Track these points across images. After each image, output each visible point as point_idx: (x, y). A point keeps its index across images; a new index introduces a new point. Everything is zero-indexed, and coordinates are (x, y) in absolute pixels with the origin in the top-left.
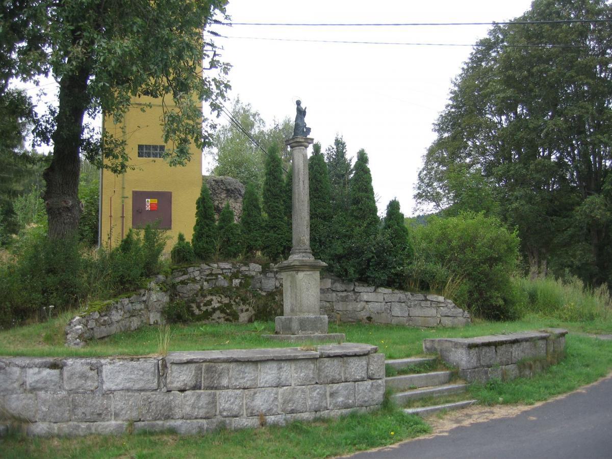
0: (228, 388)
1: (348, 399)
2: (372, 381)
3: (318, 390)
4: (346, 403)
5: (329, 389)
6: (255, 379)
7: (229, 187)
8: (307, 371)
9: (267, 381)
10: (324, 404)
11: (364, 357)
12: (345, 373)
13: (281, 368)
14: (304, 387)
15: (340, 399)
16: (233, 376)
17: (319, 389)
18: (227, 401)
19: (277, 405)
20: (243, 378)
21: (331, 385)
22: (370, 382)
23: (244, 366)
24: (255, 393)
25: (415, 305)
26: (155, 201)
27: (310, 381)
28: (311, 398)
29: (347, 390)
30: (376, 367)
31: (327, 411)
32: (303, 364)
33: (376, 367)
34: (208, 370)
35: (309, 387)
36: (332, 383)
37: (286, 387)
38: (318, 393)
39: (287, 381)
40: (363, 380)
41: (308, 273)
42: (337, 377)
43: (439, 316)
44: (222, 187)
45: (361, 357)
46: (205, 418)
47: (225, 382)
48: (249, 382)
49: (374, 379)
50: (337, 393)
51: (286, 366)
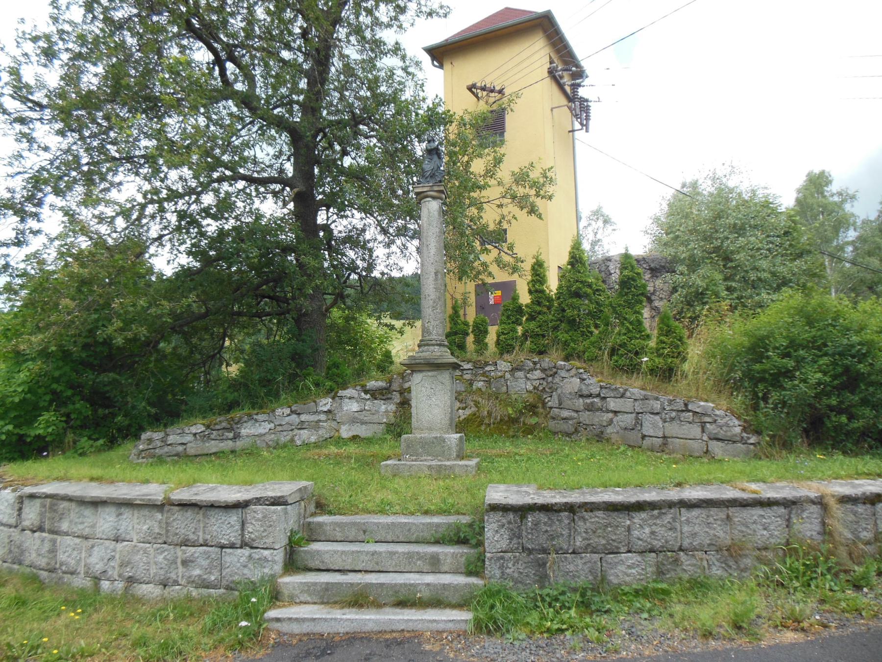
0: (67, 534)
1: (210, 573)
2: (252, 551)
3: (166, 553)
4: (205, 579)
5: (181, 553)
6: (93, 526)
7: (652, 265)
8: (151, 523)
9: (103, 531)
10: (173, 576)
11: (234, 511)
12: (205, 533)
13: (121, 514)
14: (148, 545)
15: (197, 572)
16: (74, 520)
17: (170, 552)
18: (68, 552)
19: (114, 568)
20: (82, 523)
21: (183, 548)
22: (246, 551)
23: (83, 508)
24: (93, 547)
25: (672, 419)
26: (499, 293)
27: (155, 538)
28: (156, 563)
29: (207, 558)
30: (258, 527)
31: (177, 587)
32: (146, 512)
33: (258, 527)
34: (52, 506)
35: (155, 546)
36: (186, 545)
37: (126, 543)
38: (165, 558)
39: (129, 534)
40: (232, 546)
41: (430, 374)
42: (192, 537)
43: (705, 438)
44: (645, 266)
45: (186, 508)
46: (46, 570)
47: (64, 526)
48: (87, 529)
49: (257, 548)
50: (193, 562)
51: (127, 513)
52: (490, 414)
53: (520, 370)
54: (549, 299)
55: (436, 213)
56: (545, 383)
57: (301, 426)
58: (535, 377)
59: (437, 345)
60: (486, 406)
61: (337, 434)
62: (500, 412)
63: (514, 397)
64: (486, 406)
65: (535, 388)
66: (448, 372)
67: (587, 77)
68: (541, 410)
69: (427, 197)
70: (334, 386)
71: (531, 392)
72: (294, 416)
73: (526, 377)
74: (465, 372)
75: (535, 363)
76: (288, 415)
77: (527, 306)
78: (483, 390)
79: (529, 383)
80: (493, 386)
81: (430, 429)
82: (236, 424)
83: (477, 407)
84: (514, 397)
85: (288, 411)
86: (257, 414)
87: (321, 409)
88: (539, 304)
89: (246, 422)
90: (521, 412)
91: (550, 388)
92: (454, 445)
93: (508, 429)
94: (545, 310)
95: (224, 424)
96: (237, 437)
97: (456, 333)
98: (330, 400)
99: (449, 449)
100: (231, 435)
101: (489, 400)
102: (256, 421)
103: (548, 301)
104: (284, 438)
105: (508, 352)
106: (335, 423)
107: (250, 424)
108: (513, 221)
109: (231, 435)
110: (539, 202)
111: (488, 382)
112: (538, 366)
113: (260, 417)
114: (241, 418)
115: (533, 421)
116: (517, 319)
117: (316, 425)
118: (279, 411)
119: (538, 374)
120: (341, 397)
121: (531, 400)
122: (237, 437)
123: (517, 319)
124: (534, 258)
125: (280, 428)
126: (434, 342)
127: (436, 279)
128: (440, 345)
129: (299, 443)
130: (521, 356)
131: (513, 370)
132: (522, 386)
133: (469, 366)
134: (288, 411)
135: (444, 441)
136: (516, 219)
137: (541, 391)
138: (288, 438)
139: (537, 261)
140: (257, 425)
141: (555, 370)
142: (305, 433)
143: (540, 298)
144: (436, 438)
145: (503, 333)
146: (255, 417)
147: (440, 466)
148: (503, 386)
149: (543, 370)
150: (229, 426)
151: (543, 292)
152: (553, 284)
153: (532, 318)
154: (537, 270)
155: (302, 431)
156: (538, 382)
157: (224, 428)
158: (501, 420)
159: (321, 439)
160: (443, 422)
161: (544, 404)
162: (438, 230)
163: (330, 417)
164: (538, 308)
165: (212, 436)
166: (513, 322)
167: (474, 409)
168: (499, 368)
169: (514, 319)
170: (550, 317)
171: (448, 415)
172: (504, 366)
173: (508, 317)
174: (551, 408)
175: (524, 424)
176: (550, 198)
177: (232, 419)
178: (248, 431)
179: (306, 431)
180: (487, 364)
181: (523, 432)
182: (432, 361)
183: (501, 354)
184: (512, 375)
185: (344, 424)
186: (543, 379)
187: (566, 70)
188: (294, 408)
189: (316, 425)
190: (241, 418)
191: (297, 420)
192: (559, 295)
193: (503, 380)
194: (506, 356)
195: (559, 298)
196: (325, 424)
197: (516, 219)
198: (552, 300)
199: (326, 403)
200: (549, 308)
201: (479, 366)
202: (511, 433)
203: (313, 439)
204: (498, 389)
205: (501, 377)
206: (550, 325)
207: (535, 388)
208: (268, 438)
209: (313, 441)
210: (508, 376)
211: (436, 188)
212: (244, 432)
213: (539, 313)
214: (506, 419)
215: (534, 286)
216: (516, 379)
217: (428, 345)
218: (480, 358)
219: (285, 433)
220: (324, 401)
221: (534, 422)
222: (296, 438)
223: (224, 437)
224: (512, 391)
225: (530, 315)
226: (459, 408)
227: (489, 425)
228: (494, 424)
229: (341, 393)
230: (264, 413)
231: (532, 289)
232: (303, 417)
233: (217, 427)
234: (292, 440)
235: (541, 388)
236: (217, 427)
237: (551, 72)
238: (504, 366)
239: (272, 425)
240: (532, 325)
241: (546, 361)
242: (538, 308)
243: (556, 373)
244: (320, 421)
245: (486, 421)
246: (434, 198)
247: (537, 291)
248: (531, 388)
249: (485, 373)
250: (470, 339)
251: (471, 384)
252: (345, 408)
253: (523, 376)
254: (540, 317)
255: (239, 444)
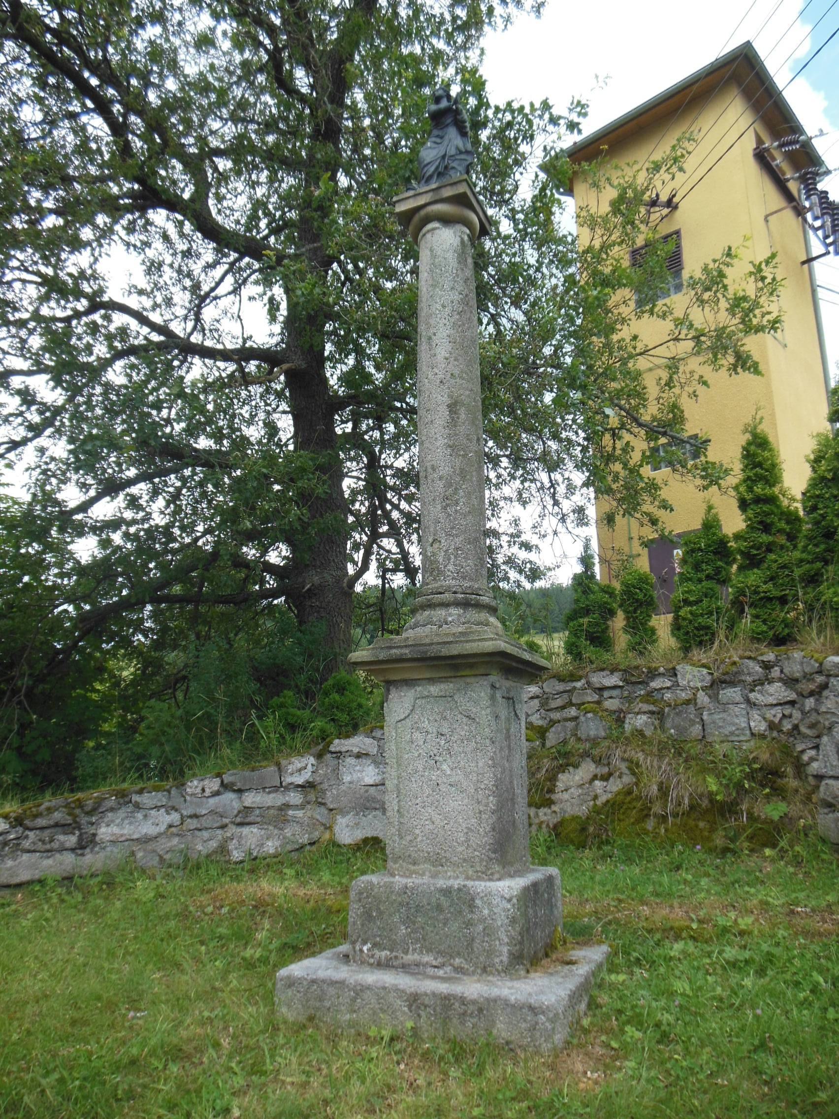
41: (434, 689)
52: (664, 790)
53: (732, 684)
54: (791, 518)
55: (452, 259)
56: (797, 714)
57: (245, 818)
58: (771, 700)
59: (457, 604)
60: (656, 771)
61: (327, 836)
62: (688, 785)
63: (721, 749)
64: (656, 771)
65: (772, 726)
66: (485, 682)
67: (828, 172)
68: (792, 783)
69: (427, 220)
70: (330, 728)
71: (762, 736)
72: (230, 796)
73: (748, 701)
74: (606, 694)
75: (767, 666)
76: (217, 794)
77: (737, 537)
78: (648, 733)
79: (755, 715)
80: (668, 724)
81: (438, 861)
82: (89, 813)
83: (634, 774)
84: (721, 749)
85: (213, 785)
86: (140, 792)
87: (288, 779)
88: (766, 528)
89: (112, 809)
90: (739, 786)
91: (812, 726)
92: (501, 920)
93: (712, 830)
94: (782, 540)
95: (57, 816)
96: (86, 843)
97: (587, 612)
98: (312, 760)
99: (489, 931)
100: (72, 840)
101: (661, 757)
102: (137, 806)
103: (788, 522)
104: (204, 845)
105: (701, 643)
106: (323, 810)
107: (121, 813)
108: (701, 390)
109: (72, 840)
110: (751, 344)
111: (660, 715)
112: (776, 672)
113: (146, 799)
114: (99, 801)
115: (774, 810)
116: (718, 571)
117: (279, 816)
118: (193, 786)
119: (776, 691)
120: (338, 755)
121: (765, 757)
122: (86, 843)
123: (718, 571)
124: (746, 431)
125: (193, 824)
126: (448, 597)
127: (453, 422)
128: (465, 604)
129: (237, 855)
130: (731, 651)
131: (715, 685)
132: (740, 722)
133: (614, 680)
134: (213, 785)
135: (471, 905)
136: (705, 383)
137: (790, 734)
138: (213, 844)
139: (755, 435)
140: (140, 816)
141: (820, 679)
142: (251, 835)
143: (767, 514)
144: (447, 892)
145: (686, 602)
146: (135, 798)
147: (446, 1000)
148: (693, 723)
149: (790, 682)
150: (69, 820)
151: (771, 500)
152: (795, 480)
153: (752, 561)
154: (754, 455)
155: (246, 830)
156: (778, 712)
157: (56, 825)
158: (692, 807)
159: (289, 847)
160: (475, 840)
161: (800, 768)
162: (456, 297)
163: (312, 797)
164: (765, 538)
165: (26, 844)
166: (708, 577)
167: (628, 779)
168: (683, 682)
169: (710, 570)
170: (797, 554)
171: (489, 820)
172: (692, 676)
173: (697, 567)
174: (820, 777)
175: (751, 817)
176: (775, 324)
177: (80, 804)
178: (115, 829)
179: (255, 829)
180: (653, 674)
181: (750, 838)
182: (433, 651)
183: (686, 650)
184: (714, 698)
185: (343, 812)
186: (792, 703)
187: (788, 158)
188: (227, 779)
189: (279, 816)
190: (99, 801)
191: (236, 805)
192: (812, 500)
193: (691, 708)
194: (698, 654)
195: (814, 508)
196: (300, 813)
197: (705, 383)
198: (798, 519)
199: (301, 768)
200: (791, 537)
201: (636, 678)
202: (719, 841)
203: (271, 847)
204: (681, 730)
205: (688, 702)
206: (797, 572)
207: (772, 726)
208: (163, 845)
209: (272, 851)
210: (703, 698)
211: (448, 192)
212: (105, 832)
213: (769, 548)
214: (705, 803)
215: (750, 489)
216: (724, 706)
217: (431, 606)
218: (640, 661)
219: (206, 834)
220: (297, 763)
221: (776, 816)
222: (231, 846)
223: (55, 845)
224: (714, 736)
225: (746, 555)
226: (595, 777)
227: (664, 818)
228: (675, 815)
229: (338, 745)
230: (157, 789)
231: (748, 497)
232: (250, 799)
233: (41, 822)
234: (223, 849)
235: (787, 726)
236: (41, 822)
237: (762, 157)
238: (692, 676)
239: (175, 817)
240: (754, 577)
241: (796, 660)
242: (765, 538)
243: (825, 686)
244: (287, 806)
245: (657, 808)
246: (447, 221)
247: (758, 500)
248: (763, 726)
249: (650, 694)
250: (619, 621)
251: (620, 721)
252: (347, 778)
253: (738, 698)
254: (772, 556)
255: (92, 860)
